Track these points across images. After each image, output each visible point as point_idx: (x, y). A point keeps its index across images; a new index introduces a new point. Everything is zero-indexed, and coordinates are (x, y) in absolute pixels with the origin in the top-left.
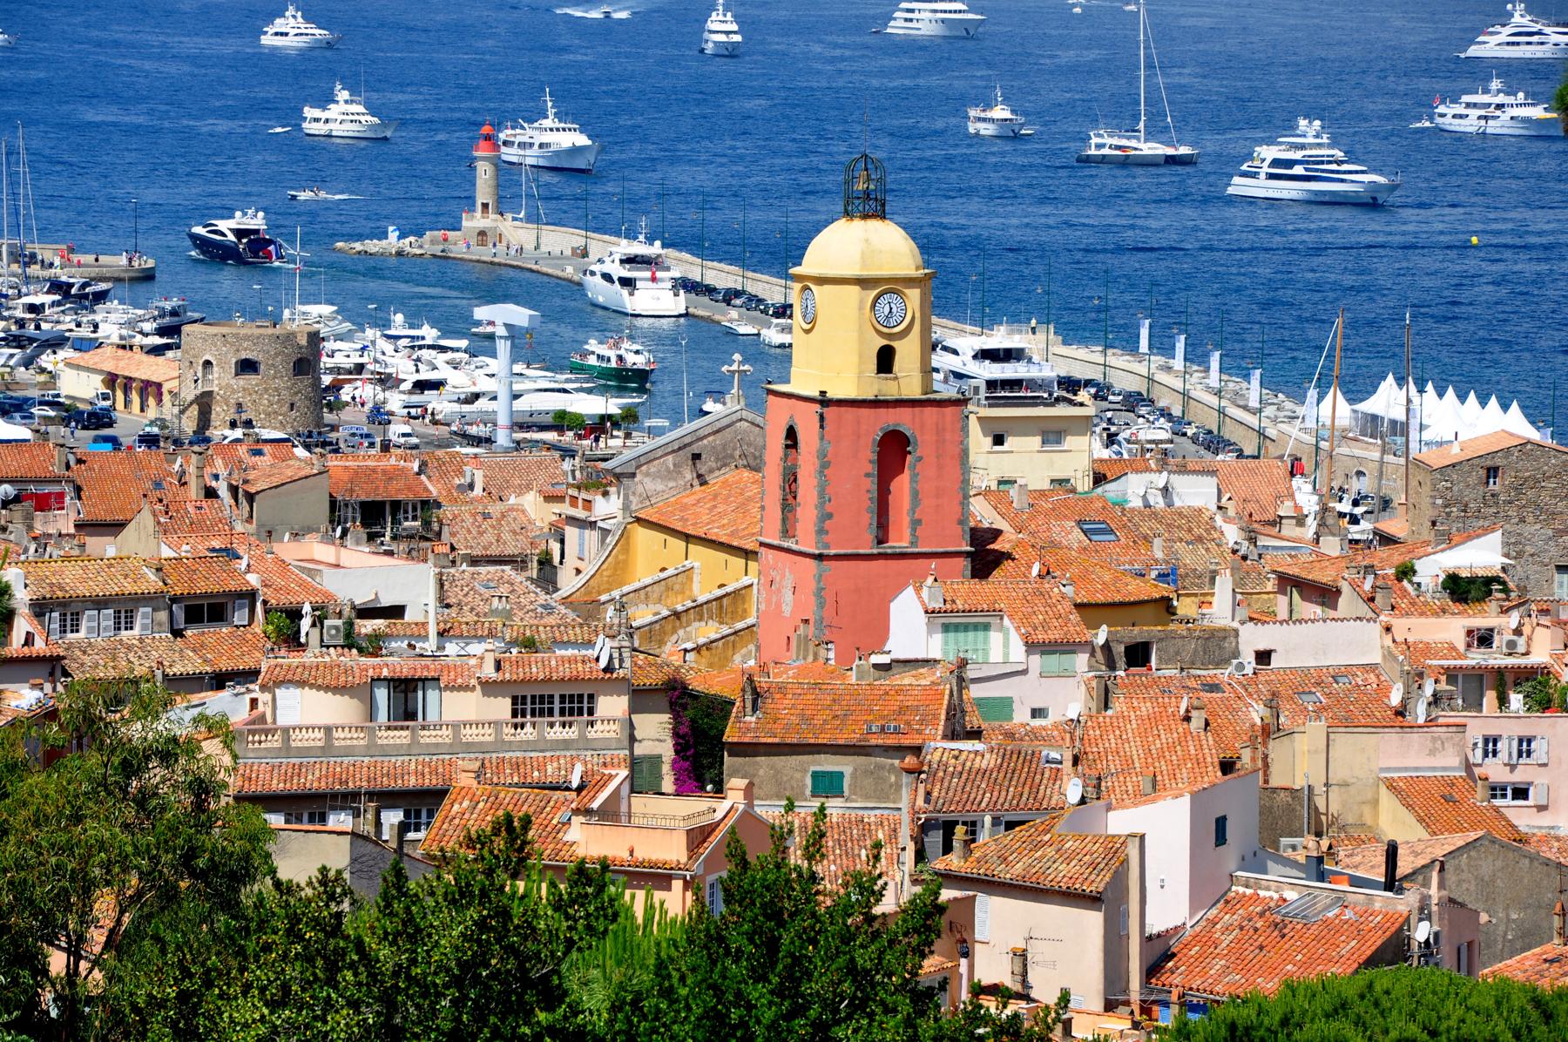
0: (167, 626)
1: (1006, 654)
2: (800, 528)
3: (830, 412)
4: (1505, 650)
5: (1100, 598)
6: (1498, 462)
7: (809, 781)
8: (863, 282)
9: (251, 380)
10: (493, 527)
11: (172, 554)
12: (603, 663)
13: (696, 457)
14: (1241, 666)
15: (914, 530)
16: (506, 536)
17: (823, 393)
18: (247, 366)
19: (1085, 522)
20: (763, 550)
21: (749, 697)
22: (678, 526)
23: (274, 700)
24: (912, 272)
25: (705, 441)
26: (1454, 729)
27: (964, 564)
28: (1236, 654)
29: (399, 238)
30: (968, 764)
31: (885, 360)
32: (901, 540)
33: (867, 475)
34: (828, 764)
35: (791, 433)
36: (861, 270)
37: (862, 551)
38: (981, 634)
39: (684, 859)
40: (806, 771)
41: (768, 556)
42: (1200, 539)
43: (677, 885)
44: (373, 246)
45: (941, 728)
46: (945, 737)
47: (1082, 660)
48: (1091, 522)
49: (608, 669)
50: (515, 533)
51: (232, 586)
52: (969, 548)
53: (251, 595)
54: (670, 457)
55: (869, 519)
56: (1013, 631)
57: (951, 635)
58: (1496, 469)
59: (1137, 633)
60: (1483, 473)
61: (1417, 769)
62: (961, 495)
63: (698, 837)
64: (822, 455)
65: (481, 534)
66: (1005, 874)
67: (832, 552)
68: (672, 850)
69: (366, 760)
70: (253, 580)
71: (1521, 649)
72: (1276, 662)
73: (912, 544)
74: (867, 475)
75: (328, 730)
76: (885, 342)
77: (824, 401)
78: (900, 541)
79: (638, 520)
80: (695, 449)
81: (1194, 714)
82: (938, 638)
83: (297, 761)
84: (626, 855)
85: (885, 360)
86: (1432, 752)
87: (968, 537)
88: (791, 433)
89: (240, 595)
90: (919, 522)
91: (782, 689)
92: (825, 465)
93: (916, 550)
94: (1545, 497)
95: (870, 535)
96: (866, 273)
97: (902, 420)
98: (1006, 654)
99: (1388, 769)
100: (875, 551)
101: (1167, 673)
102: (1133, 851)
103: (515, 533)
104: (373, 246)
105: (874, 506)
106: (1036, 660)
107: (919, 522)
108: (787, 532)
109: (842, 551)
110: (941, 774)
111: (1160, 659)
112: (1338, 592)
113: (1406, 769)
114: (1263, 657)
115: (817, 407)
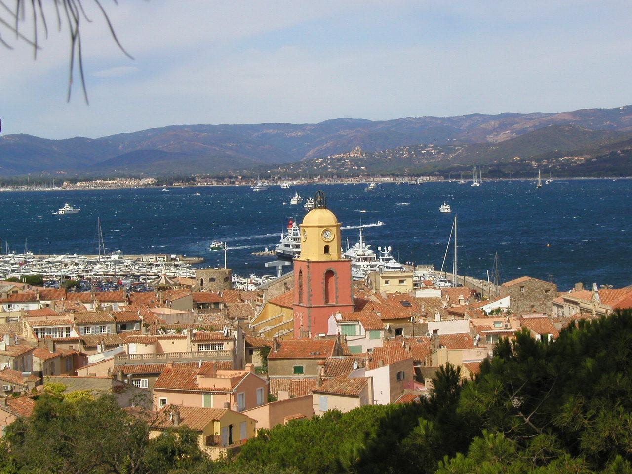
0: (115, 331)
1: (360, 333)
2: (303, 301)
3: (310, 265)
4: (504, 328)
5: (392, 318)
6: (524, 285)
7: (293, 369)
8: (319, 227)
9: (213, 283)
10: (240, 309)
11: (121, 310)
12: (225, 335)
13: (285, 284)
14: (429, 335)
15: (337, 299)
16: (243, 312)
17: (308, 259)
18: (212, 280)
19: (403, 302)
20: (295, 306)
21: (275, 345)
22: (279, 303)
23: (128, 346)
24: (334, 224)
25: (288, 279)
26: (484, 348)
27: (352, 308)
28: (428, 331)
29: (268, 251)
30: (339, 363)
31: (327, 250)
32: (333, 302)
33: (322, 283)
34: (298, 363)
35: (301, 271)
36: (319, 223)
37: (321, 305)
38: (353, 326)
39: (230, 388)
40: (292, 367)
41: (295, 307)
42: (436, 306)
43: (228, 395)
44: (262, 253)
45: (332, 353)
46: (334, 355)
47: (382, 333)
48: (404, 302)
49: (227, 336)
50: (246, 311)
51: (135, 319)
52: (353, 304)
53: (140, 322)
54: (278, 284)
55: (323, 297)
56: (362, 327)
57: (344, 327)
58: (523, 287)
59: (398, 325)
60: (520, 288)
61: (473, 361)
62: (350, 289)
63: (234, 381)
64: (309, 278)
65: (236, 311)
66: (331, 390)
67: (312, 306)
68: (227, 385)
69: (153, 364)
70: (141, 317)
71: (509, 327)
72: (439, 333)
73: (336, 303)
74: (322, 283)
75: (142, 355)
76: (327, 244)
77: (308, 261)
78: (333, 302)
79: (269, 302)
80: (285, 281)
81: (406, 345)
82: (340, 328)
83: (132, 365)
84: (213, 387)
85: (327, 250)
86: (478, 356)
87: (353, 300)
88: (301, 271)
89: (137, 322)
90: (338, 297)
91: (286, 343)
92: (309, 281)
93: (338, 305)
94: (537, 294)
95: (324, 302)
96: (320, 225)
97: (332, 267)
98: (360, 333)
99: (465, 361)
100: (325, 305)
101: (407, 337)
102: (369, 381)
103: (246, 311)
104: (262, 253)
105: (325, 292)
106: (368, 333)
107: (338, 297)
108: (300, 301)
109: (315, 306)
110: (330, 366)
111: (405, 333)
112: (464, 315)
113: (470, 361)
114: (435, 331)
115: (307, 264)
